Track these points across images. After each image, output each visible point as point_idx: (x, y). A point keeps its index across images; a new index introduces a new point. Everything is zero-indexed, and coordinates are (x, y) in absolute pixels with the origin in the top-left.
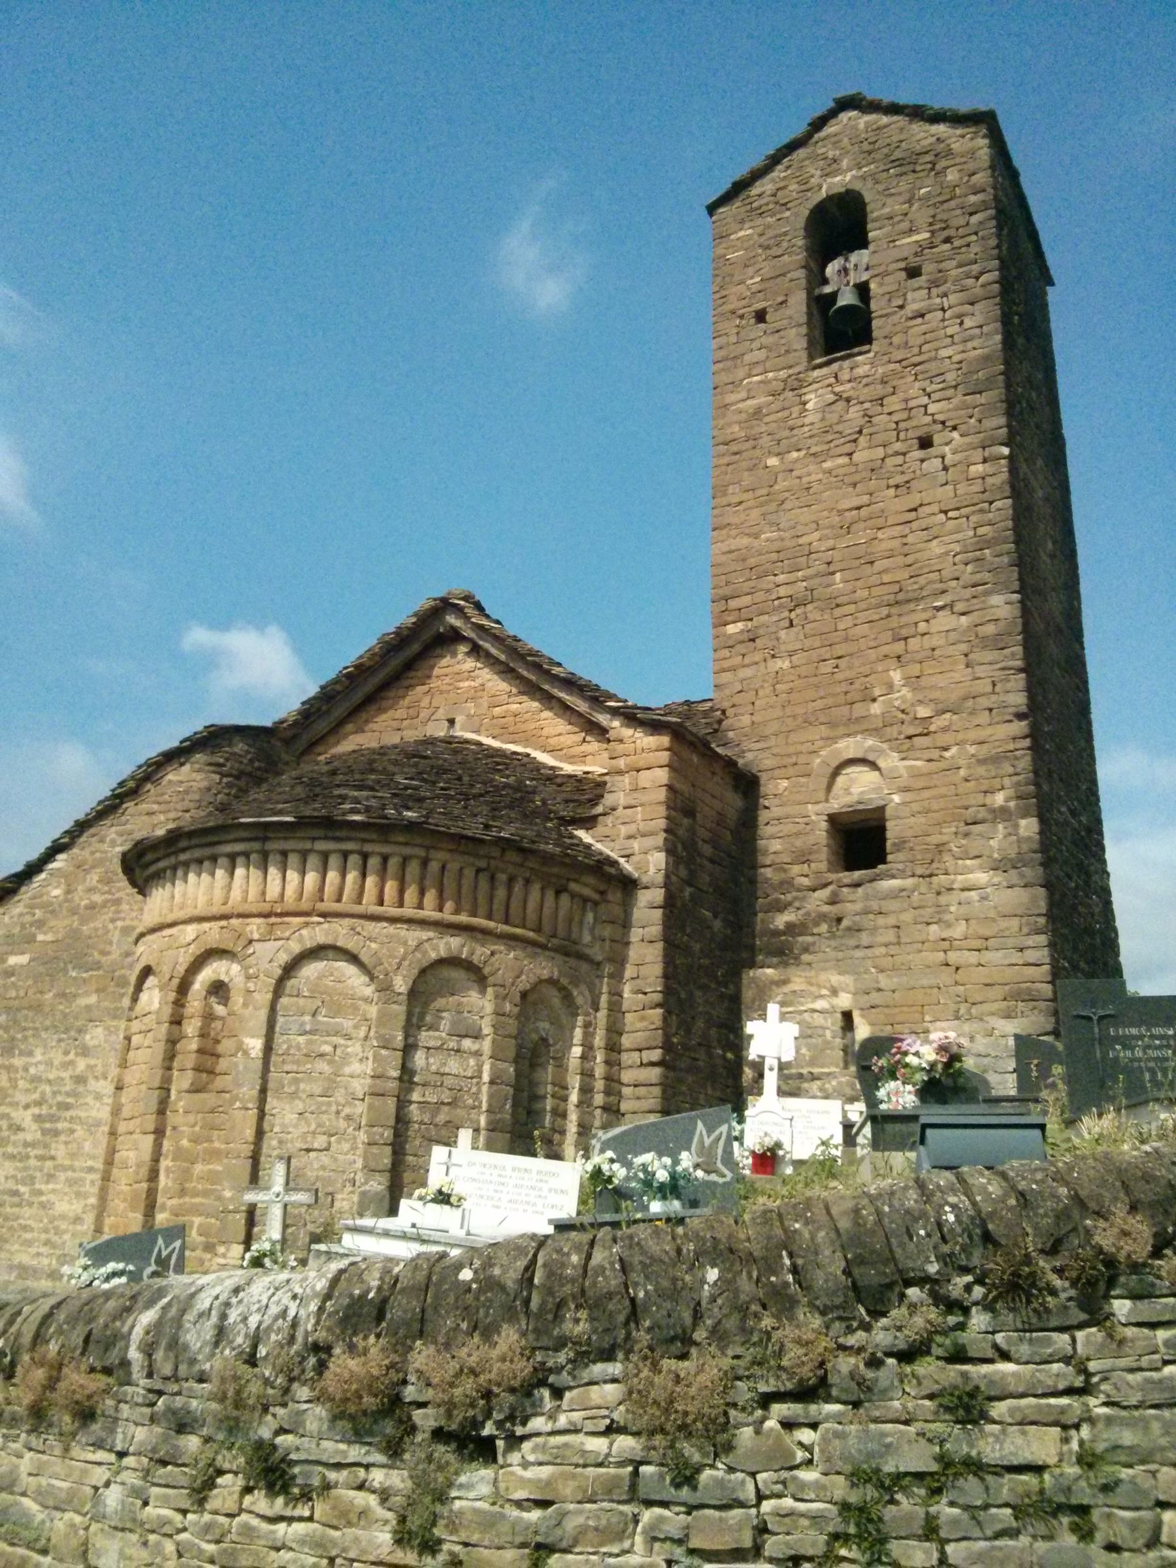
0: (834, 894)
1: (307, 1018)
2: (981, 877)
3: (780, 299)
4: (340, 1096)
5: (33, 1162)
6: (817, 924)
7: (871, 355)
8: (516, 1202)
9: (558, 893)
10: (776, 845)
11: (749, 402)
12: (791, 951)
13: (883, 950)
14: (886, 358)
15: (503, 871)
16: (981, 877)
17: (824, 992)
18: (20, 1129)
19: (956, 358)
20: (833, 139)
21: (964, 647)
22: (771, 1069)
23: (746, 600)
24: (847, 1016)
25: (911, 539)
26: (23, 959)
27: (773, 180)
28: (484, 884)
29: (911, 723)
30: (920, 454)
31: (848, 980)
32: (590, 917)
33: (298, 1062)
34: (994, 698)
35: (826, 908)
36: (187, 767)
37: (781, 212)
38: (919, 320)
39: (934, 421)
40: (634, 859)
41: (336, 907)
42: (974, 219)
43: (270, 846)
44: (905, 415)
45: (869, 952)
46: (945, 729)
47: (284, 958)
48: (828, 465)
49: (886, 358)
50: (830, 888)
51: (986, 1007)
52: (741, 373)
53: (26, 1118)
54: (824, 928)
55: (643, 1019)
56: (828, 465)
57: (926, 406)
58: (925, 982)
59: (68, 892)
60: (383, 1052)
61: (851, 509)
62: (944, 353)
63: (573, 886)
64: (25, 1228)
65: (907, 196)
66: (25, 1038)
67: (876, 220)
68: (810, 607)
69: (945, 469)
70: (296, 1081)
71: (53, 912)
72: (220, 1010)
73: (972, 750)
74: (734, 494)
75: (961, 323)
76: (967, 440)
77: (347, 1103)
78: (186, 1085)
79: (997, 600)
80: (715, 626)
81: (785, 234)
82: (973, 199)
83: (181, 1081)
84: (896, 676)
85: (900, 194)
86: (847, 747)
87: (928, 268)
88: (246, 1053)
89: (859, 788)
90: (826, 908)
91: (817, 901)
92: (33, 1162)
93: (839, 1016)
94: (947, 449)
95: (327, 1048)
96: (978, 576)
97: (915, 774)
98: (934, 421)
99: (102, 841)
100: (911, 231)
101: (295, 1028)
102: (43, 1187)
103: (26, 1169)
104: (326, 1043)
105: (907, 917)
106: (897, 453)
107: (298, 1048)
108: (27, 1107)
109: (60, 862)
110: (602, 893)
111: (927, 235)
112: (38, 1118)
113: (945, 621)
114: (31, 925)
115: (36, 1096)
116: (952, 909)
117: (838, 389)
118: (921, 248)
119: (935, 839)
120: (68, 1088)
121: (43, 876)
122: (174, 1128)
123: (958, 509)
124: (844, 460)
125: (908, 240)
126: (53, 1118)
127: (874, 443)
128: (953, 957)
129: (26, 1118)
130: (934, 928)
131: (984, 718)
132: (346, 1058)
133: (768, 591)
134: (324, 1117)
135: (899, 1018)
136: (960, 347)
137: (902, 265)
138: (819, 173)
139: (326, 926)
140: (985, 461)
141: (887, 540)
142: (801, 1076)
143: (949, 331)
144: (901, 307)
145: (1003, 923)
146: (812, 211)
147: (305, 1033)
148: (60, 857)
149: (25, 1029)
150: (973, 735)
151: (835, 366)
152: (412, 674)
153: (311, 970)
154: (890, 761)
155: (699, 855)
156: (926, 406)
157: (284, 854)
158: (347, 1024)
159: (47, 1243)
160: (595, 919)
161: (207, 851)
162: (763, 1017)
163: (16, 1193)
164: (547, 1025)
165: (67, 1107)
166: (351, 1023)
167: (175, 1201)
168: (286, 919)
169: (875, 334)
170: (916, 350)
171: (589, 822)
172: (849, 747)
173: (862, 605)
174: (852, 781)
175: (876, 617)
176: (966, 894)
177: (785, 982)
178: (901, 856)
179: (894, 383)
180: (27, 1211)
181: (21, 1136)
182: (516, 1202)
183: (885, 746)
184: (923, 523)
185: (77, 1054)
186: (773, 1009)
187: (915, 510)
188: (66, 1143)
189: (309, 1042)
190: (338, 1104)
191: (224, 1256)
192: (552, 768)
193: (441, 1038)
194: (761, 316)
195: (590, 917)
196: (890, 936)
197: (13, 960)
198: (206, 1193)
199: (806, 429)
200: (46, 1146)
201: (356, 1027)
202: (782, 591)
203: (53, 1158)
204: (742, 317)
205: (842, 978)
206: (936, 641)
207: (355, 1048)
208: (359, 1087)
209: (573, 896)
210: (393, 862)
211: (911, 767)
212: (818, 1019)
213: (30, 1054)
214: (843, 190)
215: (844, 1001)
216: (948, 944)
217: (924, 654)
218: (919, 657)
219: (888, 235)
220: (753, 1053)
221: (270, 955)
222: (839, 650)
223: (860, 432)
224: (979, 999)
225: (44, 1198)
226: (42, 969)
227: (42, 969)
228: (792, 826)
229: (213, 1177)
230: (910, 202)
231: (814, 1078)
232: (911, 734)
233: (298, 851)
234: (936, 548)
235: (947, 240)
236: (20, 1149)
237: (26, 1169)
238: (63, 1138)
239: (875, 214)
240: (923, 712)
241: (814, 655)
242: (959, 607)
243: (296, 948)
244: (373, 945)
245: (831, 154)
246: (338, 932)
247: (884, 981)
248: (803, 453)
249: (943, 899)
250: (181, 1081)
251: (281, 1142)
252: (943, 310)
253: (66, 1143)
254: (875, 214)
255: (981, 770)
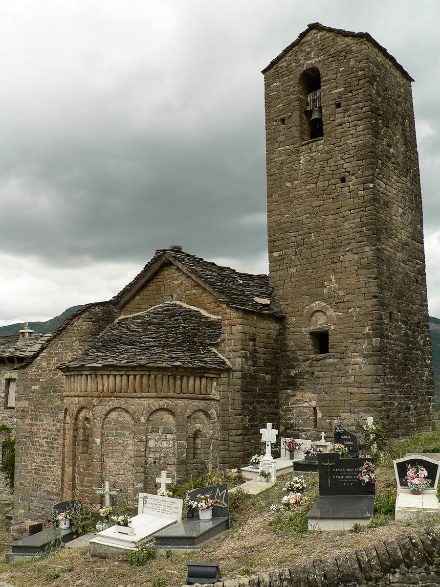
0: (311, 364)
1: (114, 431)
2: (359, 360)
3: (290, 114)
4: (126, 457)
5: (47, 457)
6: (305, 375)
7: (323, 141)
8: (164, 510)
9: (201, 378)
10: (291, 343)
11: (279, 158)
12: (297, 385)
13: (327, 385)
14: (328, 143)
15: (178, 375)
16: (359, 360)
17: (307, 400)
18: (42, 445)
19: (354, 144)
20: (308, 43)
21: (356, 268)
22: (268, 446)
23: (280, 242)
24: (315, 408)
25: (338, 221)
26: (37, 387)
27: (286, 60)
28: (172, 381)
29: (338, 298)
30: (340, 185)
31: (315, 396)
32: (215, 384)
33: (112, 446)
34: (366, 289)
35: (308, 369)
36: (80, 320)
37: (290, 75)
38: (341, 127)
39: (346, 171)
40: (232, 360)
41: (119, 394)
42: (362, 82)
43: (97, 372)
44: (335, 168)
45: (322, 386)
46: (349, 301)
47: (104, 412)
48: (308, 187)
49: (328, 143)
50: (310, 361)
51: (359, 409)
52: (276, 145)
53: (43, 442)
54: (307, 376)
55: (235, 419)
56: (308, 187)
57: (343, 164)
58: (340, 398)
59: (48, 364)
60: (139, 443)
61: (317, 207)
62: (349, 142)
63: (206, 375)
64: (47, 479)
65: (335, 71)
66: (41, 415)
67: (324, 81)
68: (303, 247)
69: (350, 192)
70: (113, 452)
71: (44, 371)
72: (88, 426)
73: (358, 310)
74: (275, 197)
75: (356, 129)
76: (358, 180)
77: (129, 459)
78: (80, 451)
79: (367, 249)
80: (269, 253)
81: (291, 85)
82: (360, 73)
83: (79, 450)
84: (332, 277)
85: (333, 70)
86: (316, 305)
87: (343, 104)
88: (96, 443)
89: (320, 322)
90: (308, 369)
91: (304, 366)
92: (47, 457)
93: (312, 409)
94: (350, 183)
95: (122, 442)
96: (361, 238)
97: (338, 317)
98: (346, 171)
99: (57, 346)
100: (336, 87)
101: (111, 434)
102: (51, 465)
103: (45, 459)
104: (121, 440)
105: (335, 373)
106: (332, 184)
107: (112, 441)
108: (43, 438)
109: (44, 353)
110: (219, 374)
111: (343, 89)
112: (47, 443)
113: (350, 256)
114: (38, 375)
115: (46, 435)
116: (350, 371)
117: (311, 155)
118: (340, 95)
119: (345, 344)
120: (55, 433)
121: (39, 358)
122: (78, 465)
123: (354, 209)
124: (313, 186)
125: (336, 91)
126: (52, 443)
127: (324, 179)
128: (350, 389)
129: (43, 442)
130: (344, 378)
131: (362, 297)
132: (127, 446)
133: (288, 239)
134: (122, 464)
135: (332, 411)
136: (355, 140)
137: (334, 102)
138: (303, 58)
139: (117, 401)
140: (364, 190)
141: (330, 220)
142: (299, 430)
143: (351, 132)
144: (334, 120)
145: (366, 378)
146: (301, 75)
147: (114, 436)
148: (44, 351)
149: (40, 412)
150: (358, 303)
151: (310, 145)
152: (157, 277)
153: (113, 415)
154: (331, 312)
155: (258, 353)
156: (343, 164)
157: (102, 375)
158: (127, 433)
159: (54, 484)
160: (217, 385)
161: (79, 373)
162: (265, 427)
163: (43, 467)
164: (199, 425)
165: (56, 439)
166: (128, 433)
167: (81, 488)
168: (105, 398)
169: (325, 131)
170: (339, 140)
171: (216, 345)
172: (316, 305)
173: (321, 248)
174: (318, 319)
175: (326, 253)
176: (355, 366)
177: (294, 396)
178: (333, 350)
179: (331, 154)
180: (47, 473)
181: (43, 448)
182: (164, 510)
183: (328, 306)
184: (342, 214)
185: (56, 422)
186: (269, 425)
187: (339, 209)
188: (56, 451)
189: (115, 439)
190: (126, 459)
191: (95, 507)
192: (207, 318)
193: (159, 435)
194: (283, 121)
195: (215, 384)
196: (329, 380)
197: (34, 387)
198: (88, 487)
199: (300, 171)
200: (51, 452)
201: (130, 434)
202: (293, 239)
203: (53, 456)
204: (276, 121)
205: (313, 395)
206: (346, 264)
207: (130, 442)
208: (131, 453)
209: (207, 378)
210: (138, 377)
211: (338, 315)
212: (305, 410)
213: (42, 421)
214: (311, 67)
215: (314, 403)
216: (349, 385)
217: (341, 270)
218: (340, 270)
219: (328, 88)
220: (263, 439)
221: (100, 410)
222: (314, 265)
223: (320, 174)
224: (357, 406)
225: (52, 469)
226: (42, 391)
227: (42, 391)
228: (299, 335)
229: (91, 482)
230: (336, 73)
231: (303, 431)
232: (337, 303)
233: (107, 374)
234: (346, 225)
235: (351, 92)
236: (43, 452)
237: (45, 459)
238: (55, 450)
239: (324, 79)
240: (342, 293)
241: (304, 266)
242: (355, 251)
243: (108, 408)
244: (133, 407)
245: (307, 50)
246: (121, 402)
247: (327, 398)
248: (299, 181)
249: (347, 367)
250: (79, 450)
251: (109, 472)
252: (349, 122)
253: (56, 451)
254: (324, 79)
255: (361, 318)
